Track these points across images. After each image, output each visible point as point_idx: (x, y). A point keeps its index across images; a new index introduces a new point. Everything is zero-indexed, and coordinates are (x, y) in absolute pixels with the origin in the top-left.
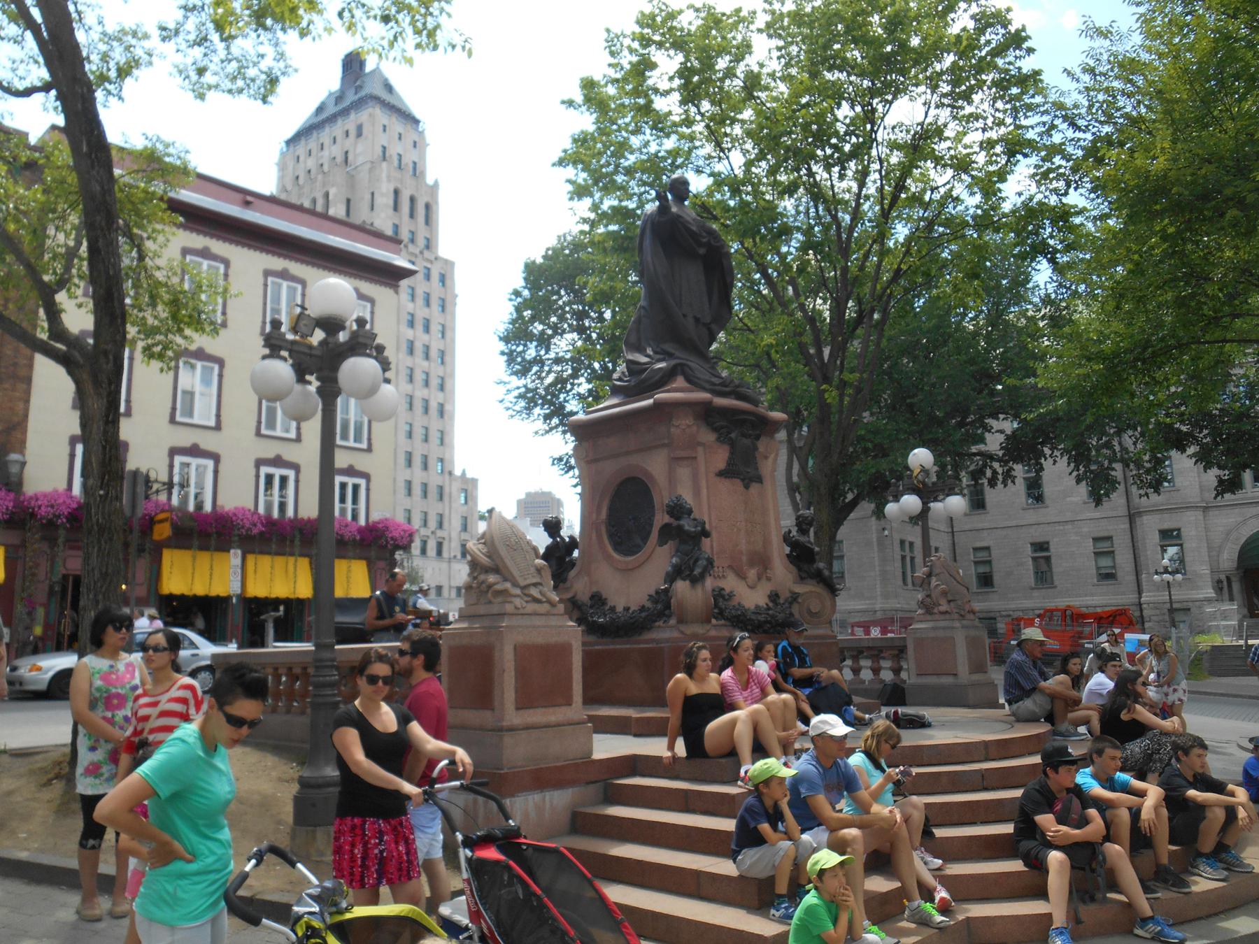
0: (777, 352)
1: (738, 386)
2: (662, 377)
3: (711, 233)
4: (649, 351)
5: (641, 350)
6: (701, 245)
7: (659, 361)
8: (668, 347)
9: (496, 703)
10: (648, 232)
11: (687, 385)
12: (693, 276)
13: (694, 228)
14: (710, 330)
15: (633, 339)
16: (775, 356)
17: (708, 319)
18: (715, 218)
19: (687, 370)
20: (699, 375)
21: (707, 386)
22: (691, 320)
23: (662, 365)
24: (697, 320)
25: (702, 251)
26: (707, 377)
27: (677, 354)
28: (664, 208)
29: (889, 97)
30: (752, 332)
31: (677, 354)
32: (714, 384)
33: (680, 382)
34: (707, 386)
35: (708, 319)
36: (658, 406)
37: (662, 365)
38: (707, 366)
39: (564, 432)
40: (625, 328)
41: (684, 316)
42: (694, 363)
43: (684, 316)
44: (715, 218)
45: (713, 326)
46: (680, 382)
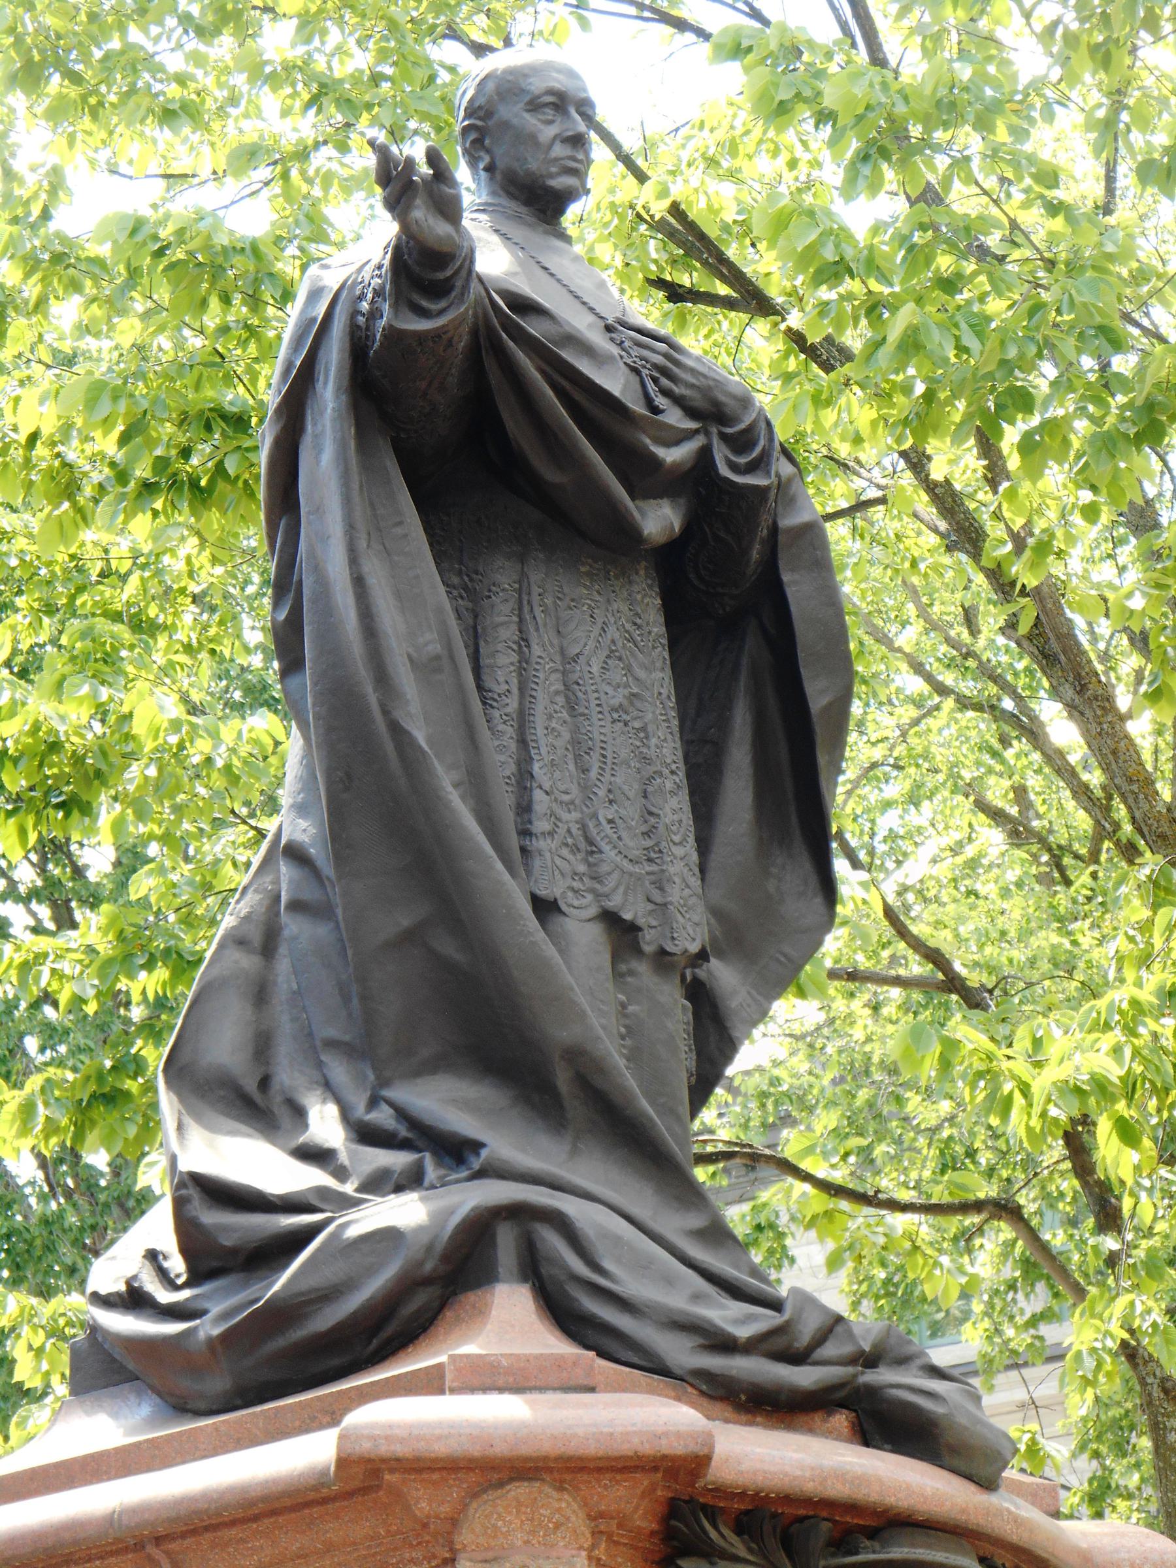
0: (1127, 1133)
1: (870, 1360)
2: (407, 1285)
3: (716, 410)
4: (325, 1124)
5: (258, 1105)
6: (643, 475)
7: (380, 1183)
8: (445, 1101)
9: (445, 249)
10: (329, 395)
11: (552, 1344)
12: (601, 665)
13: (614, 382)
14: (701, 996)
15: (225, 1048)
16: (1114, 1157)
17: (690, 934)
18: (753, 300)
19: (552, 1241)
20: (631, 1286)
21: (681, 1352)
22: (584, 936)
23: (406, 1212)
24: (621, 932)
25: (659, 519)
26: (682, 1294)
27: (503, 1143)
28: (426, 267)
29: (148, 983)
30: (973, 1000)
31: (503, 1143)
32: (724, 1344)
33: (508, 1322)
34: (681, 1352)
35: (690, 934)
36: (366, 1478)
37: (406, 1212)
38: (675, 1224)
39: (616, 246)
40: (182, 964)
41: (545, 908)
42: (601, 1203)
43: (545, 908)
44: (753, 300)
45: (723, 974)
46: (508, 1322)
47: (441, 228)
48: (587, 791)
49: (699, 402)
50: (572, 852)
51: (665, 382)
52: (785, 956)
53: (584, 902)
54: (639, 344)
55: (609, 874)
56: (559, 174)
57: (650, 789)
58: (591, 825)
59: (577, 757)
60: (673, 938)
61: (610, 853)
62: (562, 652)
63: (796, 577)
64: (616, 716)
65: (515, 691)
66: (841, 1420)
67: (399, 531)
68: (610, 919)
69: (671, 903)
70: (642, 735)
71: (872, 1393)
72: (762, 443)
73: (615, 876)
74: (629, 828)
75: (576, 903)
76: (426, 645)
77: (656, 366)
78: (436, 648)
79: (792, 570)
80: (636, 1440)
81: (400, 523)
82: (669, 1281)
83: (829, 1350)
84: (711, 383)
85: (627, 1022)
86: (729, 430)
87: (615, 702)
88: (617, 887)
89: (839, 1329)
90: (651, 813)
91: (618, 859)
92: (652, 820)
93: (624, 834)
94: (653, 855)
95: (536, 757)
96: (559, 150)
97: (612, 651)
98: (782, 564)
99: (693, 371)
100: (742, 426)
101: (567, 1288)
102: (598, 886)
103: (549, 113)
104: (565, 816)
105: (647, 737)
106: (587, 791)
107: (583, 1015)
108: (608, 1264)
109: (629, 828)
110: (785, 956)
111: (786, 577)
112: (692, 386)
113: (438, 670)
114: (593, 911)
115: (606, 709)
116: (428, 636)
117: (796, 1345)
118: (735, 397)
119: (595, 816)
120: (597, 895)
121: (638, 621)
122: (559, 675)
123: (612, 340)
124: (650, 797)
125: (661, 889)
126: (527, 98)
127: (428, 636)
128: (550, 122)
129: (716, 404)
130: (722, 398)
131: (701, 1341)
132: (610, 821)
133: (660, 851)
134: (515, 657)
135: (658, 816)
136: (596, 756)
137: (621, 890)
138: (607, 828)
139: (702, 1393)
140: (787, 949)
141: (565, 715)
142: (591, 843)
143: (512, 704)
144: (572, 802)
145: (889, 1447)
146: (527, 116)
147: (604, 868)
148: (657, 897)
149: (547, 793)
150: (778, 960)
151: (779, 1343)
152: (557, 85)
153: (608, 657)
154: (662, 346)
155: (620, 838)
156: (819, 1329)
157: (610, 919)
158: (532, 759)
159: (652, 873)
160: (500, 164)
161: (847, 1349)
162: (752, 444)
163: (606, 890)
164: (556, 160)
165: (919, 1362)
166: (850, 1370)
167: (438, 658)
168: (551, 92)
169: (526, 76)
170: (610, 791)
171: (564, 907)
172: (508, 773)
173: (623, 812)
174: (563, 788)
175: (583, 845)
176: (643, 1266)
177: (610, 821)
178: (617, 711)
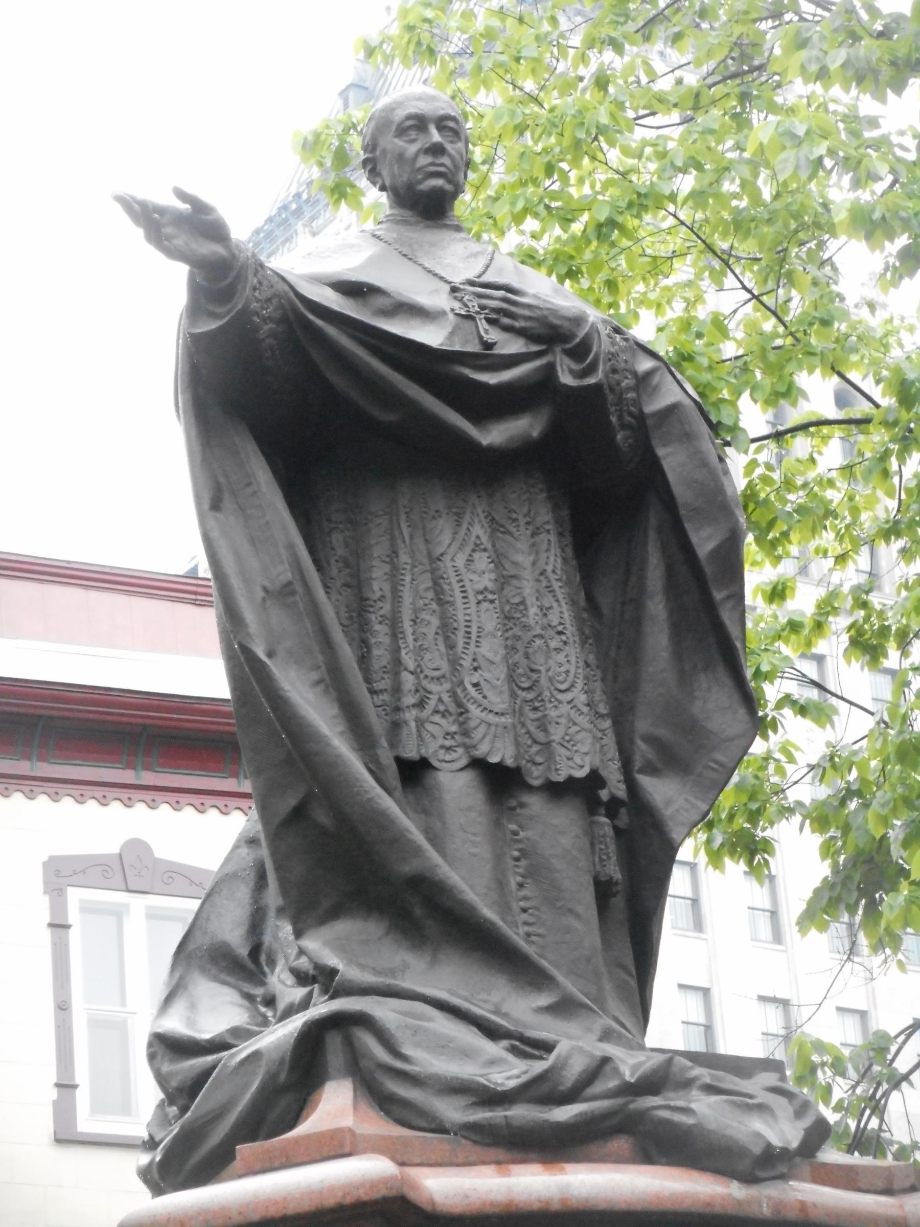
21: (453, 1111)
34: (453, 1111)
47: (218, 249)
48: (455, 663)
49: (542, 331)
50: (444, 716)
51: (506, 321)
52: (716, 762)
53: (454, 755)
54: (480, 296)
55: (476, 728)
56: (425, 179)
57: (530, 651)
58: (459, 691)
59: (446, 638)
60: (557, 770)
61: (475, 711)
62: (429, 554)
63: (669, 450)
64: (481, 597)
65: (388, 595)
66: (621, 1144)
67: (249, 490)
68: (478, 764)
69: (553, 741)
70: (522, 607)
71: (642, 1115)
72: (595, 349)
73: (482, 729)
74: (494, 687)
75: (448, 758)
76: (279, 575)
77: (498, 311)
78: (289, 576)
79: (665, 445)
80: (340, 1194)
81: (249, 484)
82: (466, 1054)
83: (598, 1087)
84: (545, 312)
85: (520, 846)
86: (568, 346)
87: (480, 587)
88: (484, 737)
89: (608, 1068)
90: (532, 670)
91: (483, 715)
92: (535, 676)
93: (488, 693)
94: (537, 704)
95: (402, 646)
96: (424, 160)
97: (476, 545)
98: (654, 442)
99: (529, 306)
100: (578, 340)
101: (376, 1075)
102: (467, 741)
103: (413, 134)
104: (433, 687)
105: (526, 609)
106: (455, 663)
107: (417, 851)
108: (407, 1050)
109: (494, 687)
110: (716, 762)
111: (661, 452)
112: (529, 318)
113: (293, 593)
114: (464, 762)
115: (471, 594)
116: (280, 568)
117: (561, 1088)
118: (569, 319)
119: (461, 683)
120: (467, 748)
121: (514, 516)
122: (428, 575)
123: (455, 298)
124: (532, 657)
125: (545, 730)
126: (394, 127)
127: (280, 568)
128: (413, 141)
129: (554, 327)
130: (557, 322)
131: (473, 1099)
132: (476, 685)
133: (543, 700)
134: (387, 568)
135: (539, 671)
136: (461, 633)
137: (488, 738)
138: (472, 691)
139: (475, 1142)
140: (719, 757)
141: (434, 606)
142: (459, 704)
143: (386, 608)
144: (443, 676)
145: (664, 1160)
146: (396, 140)
147: (472, 724)
148: (540, 736)
149: (412, 673)
150: (713, 769)
151: (544, 1088)
152: (413, 110)
153: (473, 551)
154: (501, 293)
155: (485, 697)
156: (585, 1071)
157: (478, 764)
158: (399, 648)
159: (537, 720)
160: (387, 184)
161: (612, 1084)
162: (588, 351)
163: (474, 741)
164: (420, 169)
165: (698, 1083)
166: (619, 1101)
167: (290, 583)
168: (409, 117)
169: (393, 109)
170: (474, 660)
171: (435, 763)
172: (384, 663)
173: (487, 675)
174: (434, 666)
175: (452, 708)
176: (443, 1046)
177: (476, 685)
178: (482, 593)
